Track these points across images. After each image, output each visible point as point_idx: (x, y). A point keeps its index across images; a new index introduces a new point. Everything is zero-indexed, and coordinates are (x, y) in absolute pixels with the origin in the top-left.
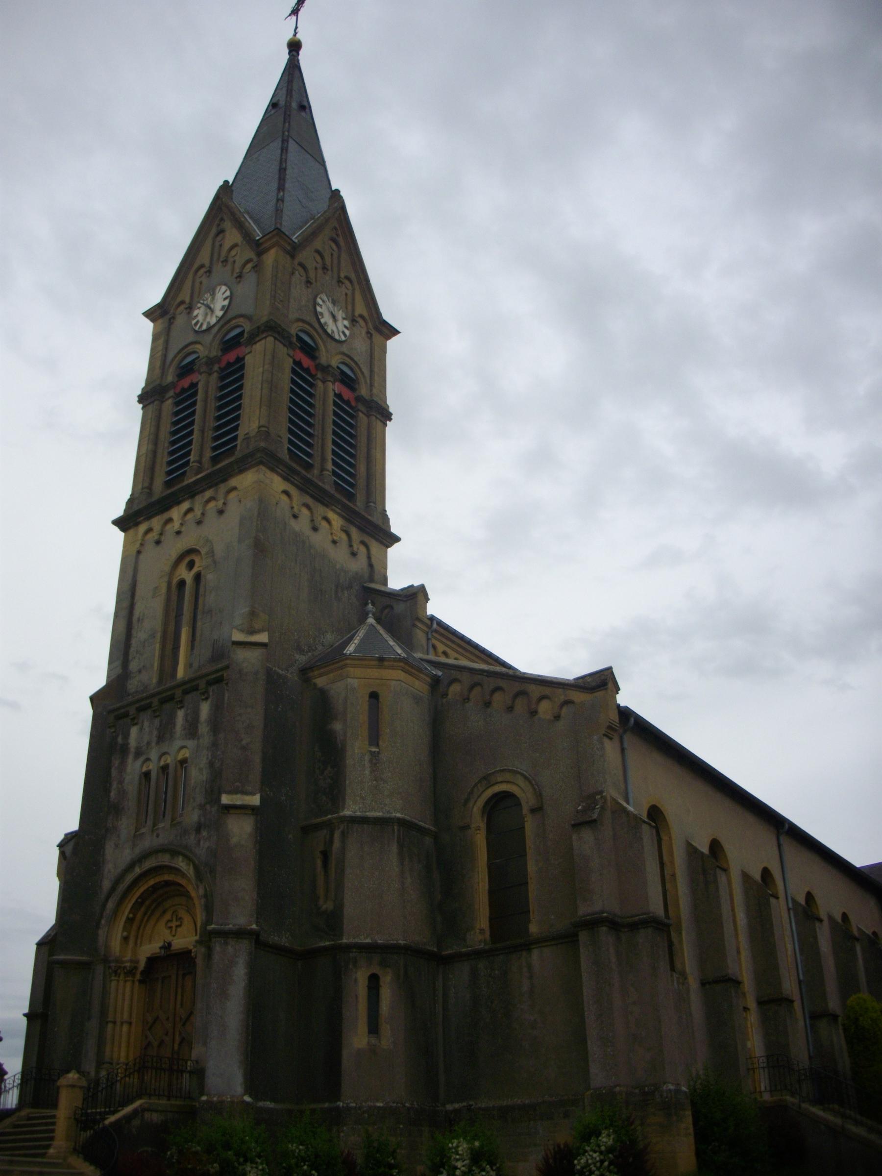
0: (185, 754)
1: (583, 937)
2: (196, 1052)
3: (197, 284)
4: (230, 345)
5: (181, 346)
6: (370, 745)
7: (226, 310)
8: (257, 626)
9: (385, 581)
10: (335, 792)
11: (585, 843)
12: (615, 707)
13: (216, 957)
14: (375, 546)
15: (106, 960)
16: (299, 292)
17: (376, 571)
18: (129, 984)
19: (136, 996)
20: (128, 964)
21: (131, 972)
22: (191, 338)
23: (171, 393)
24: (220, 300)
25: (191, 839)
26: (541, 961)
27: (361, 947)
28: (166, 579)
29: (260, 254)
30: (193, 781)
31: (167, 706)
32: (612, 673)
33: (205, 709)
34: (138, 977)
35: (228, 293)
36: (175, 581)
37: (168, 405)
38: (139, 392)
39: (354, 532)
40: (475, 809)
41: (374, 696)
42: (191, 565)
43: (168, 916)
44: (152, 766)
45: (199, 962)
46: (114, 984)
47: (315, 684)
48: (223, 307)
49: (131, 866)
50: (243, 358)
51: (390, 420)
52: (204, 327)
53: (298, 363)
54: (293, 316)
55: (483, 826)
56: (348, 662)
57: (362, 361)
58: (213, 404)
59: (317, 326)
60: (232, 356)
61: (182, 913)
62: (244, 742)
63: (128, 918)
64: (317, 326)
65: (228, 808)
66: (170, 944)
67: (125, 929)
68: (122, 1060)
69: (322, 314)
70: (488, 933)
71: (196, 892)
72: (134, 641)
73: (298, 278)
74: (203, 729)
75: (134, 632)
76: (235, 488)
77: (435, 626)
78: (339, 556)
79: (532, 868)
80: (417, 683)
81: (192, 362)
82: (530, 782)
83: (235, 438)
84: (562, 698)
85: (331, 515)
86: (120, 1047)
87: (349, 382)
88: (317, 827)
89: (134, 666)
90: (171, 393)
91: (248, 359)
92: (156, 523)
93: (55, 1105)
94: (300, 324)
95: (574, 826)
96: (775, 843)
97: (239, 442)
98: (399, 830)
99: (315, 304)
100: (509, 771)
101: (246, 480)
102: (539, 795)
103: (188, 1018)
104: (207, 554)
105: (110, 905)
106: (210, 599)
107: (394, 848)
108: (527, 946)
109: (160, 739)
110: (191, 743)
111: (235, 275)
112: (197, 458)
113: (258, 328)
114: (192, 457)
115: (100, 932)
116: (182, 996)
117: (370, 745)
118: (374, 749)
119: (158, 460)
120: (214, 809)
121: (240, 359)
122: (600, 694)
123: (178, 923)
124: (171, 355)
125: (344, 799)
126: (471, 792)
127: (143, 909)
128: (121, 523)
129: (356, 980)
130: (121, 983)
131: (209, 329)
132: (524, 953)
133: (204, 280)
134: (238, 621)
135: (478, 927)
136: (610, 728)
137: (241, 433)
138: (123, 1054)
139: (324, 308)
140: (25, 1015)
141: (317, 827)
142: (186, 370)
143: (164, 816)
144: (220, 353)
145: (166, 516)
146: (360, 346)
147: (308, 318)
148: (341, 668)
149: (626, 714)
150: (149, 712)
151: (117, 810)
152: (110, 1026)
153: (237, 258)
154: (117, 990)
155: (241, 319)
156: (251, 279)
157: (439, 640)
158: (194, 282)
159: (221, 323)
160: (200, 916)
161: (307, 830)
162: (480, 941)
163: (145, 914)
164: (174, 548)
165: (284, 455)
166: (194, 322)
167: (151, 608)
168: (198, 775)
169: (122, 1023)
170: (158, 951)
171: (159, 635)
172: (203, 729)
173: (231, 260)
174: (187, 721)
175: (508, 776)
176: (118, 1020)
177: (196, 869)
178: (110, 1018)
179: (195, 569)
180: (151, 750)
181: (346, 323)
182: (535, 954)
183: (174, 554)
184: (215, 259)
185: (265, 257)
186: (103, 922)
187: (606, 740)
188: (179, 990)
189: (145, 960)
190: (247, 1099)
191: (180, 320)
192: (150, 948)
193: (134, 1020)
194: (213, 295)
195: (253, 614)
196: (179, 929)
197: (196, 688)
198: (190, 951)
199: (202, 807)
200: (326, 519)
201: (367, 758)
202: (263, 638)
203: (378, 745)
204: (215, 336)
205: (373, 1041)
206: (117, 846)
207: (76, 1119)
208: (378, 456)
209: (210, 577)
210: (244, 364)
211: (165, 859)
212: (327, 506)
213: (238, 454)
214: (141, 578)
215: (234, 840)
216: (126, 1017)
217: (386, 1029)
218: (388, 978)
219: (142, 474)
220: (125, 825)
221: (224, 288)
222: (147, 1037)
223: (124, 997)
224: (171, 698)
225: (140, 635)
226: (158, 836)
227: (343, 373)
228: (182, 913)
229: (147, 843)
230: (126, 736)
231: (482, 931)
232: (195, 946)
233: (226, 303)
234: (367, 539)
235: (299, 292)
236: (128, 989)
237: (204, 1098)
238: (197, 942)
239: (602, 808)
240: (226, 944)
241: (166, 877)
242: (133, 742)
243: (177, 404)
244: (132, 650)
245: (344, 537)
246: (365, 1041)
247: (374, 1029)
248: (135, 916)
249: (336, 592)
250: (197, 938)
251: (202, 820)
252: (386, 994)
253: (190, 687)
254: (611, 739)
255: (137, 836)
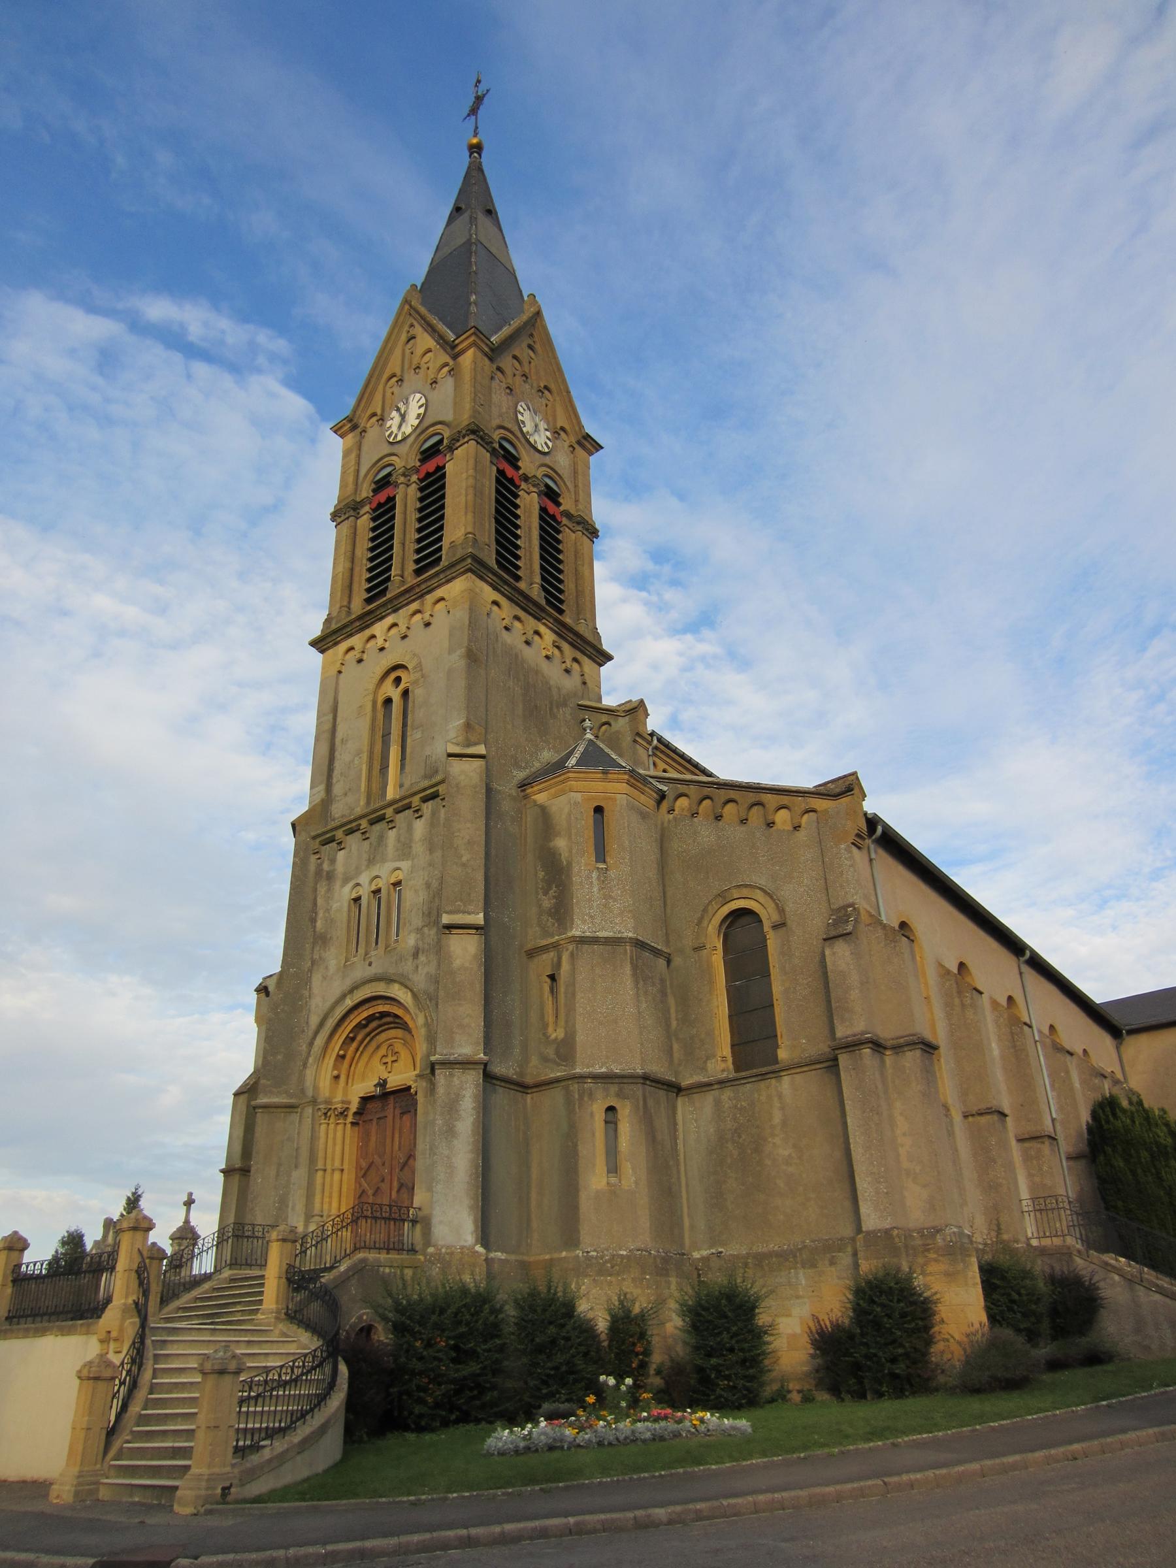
0: (399, 875)
1: (844, 1060)
2: (419, 1199)
3: (388, 394)
4: (428, 454)
5: (374, 460)
6: (597, 861)
7: (421, 418)
8: (473, 739)
9: (600, 699)
10: (561, 912)
11: (840, 956)
12: (862, 815)
13: (441, 1090)
14: (588, 664)
15: (314, 1102)
16: (500, 398)
17: (590, 687)
18: (340, 1127)
19: (347, 1141)
20: (339, 1106)
21: (343, 1114)
22: (387, 449)
23: (367, 508)
24: (414, 409)
25: (407, 967)
26: (789, 1095)
27: (596, 1077)
28: (371, 697)
29: (455, 357)
30: (408, 904)
31: (377, 827)
32: (857, 778)
33: (420, 827)
34: (350, 1119)
35: (423, 401)
36: (380, 700)
37: (365, 522)
38: (332, 510)
39: (566, 647)
40: (710, 927)
41: (599, 810)
42: (398, 680)
43: (382, 1051)
44: (364, 892)
45: (420, 1098)
46: (323, 1127)
47: (535, 801)
48: (419, 415)
49: (343, 997)
50: (444, 467)
51: (597, 537)
52: (399, 438)
53: (501, 472)
54: (496, 422)
55: (720, 946)
56: (570, 775)
57: (566, 473)
58: (413, 516)
59: (520, 435)
60: (431, 466)
61: (398, 1046)
62: (464, 859)
63: (338, 1055)
64: (520, 435)
65: (449, 927)
66: (385, 1081)
67: (335, 1067)
68: (334, 1212)
69: (523, 422)
70: (730, 1060)
71: (418, 1021)
72: (338, 765)
73: (498, 386)
74: (419, 848)
75: (337, 754)
76: (442, 599)
77: (655, 742)
78: (553, 673)
79: (777, 988)
80: (643, 798)
81: (389, 474)
82: (771, 897)
83: (440, 549)
84: (803, 807)
85: (542, 629)
86: (331, 1197)
87: (551, 495)
88: (544, 949)
89: (338, 789)
90: (367, 508)
91: (449, 468)
92: (357, 641)
93: (264, 1265)
94: (502, 431)
95: (825, 940)
96: (1016, 971)
97: (444, 552)
98: (632, 951)
99: (516, 412)
100: (746, 886)
101: (457, 587)
102: (781, 911)
103: (405, 1164)
104: (415, 668)
105: (320, 1041)
106: (418, 714)
107: (628, 970)
108: (776, 1074)
109: (371, 862)
110: (405, 865)
111: (430, 381)
112: (399, 572)
113: (459, 432)
114: (393, 572)
115: (308, 1072)
116: (400, 1137)
117: (597, 861)
118: (602, 866)
119: (356, 579)
120: (433, 932)
121: (440, 468)
122: (844, 800)
123: (394, 1058)
124: (363, 472)
125: (572, 920)
126: (705, 910)
127: (355, 1045)
128: (321, 644)
129: (592, 1115)
130: (332, 1126)
131: (404, 439)
132: (773, 1081)
133: (396, 390)
134: (452, 734)
135: (719, 1054)
136: (858, 835)
137: (445, 543)
138: (335, 1204)
139: (526, 417)
140: (222, 1171)
141: (544, 949)
142: (383, 484)
143: (377, 943)
144: (418, 464)
145: (367, 633)
146: (562, 461)
147: (509, 426)
148: (563, 782)
149: (872, 822)
150: (358, 834)
151: (322, 940)
152: (320, 1173)
153: (430, 365)
154: (327, 1134)
155: (439, 426)
156: (447, 385)
157: (660, 758)
158: (384, 392)
159: (418, 431)
160: (421, 1048)
161: (532, 953)
162: (723, 1071)
163: (357, 1050)
164: (378, 664)
165: (493, 563)
166: (387, 434)
167: (356, 731)
168: (415, 897)
169: (333, 1170)
170: (373, 1089)
171: (365, 756)
172: (419, 848)
173: (424, 367)
174: (399, 841)
175: (745, 892)
176: (329, 1167)
177: (415, 995)
178: (320, 1165)
179: (402, 686)
180: (359, 872)
181: (548, 434)
182: (786, 1080)
183: (379, 671)
184: (406, 366)
185: (461, 359)
186: (311, 1060)
187: (854, 849)
188: (397, 1135)
189: (358, 1100)
190: (479, 1248)
191: (373, 433)
192: (366, 1086)
193: (346, 1167)
194: (406, 403)
195: (468, 726)
196: (395, 1064)
197: (408, 807)
198: (409, 1088)
199: (419, 930)
200: (537, 633)
201: (595, 875)
202: (481, 749)
203: (604, 861)
204: (411, 446)
205: (613, 1180)
206: (324, 978)
207: (288, 1279)
208: (587, 573)
209: (417, 693)
210: (445, 474)
211: (380, 989)
212: (539, 620)
213: (444, 563)
214: (342, 698)
215: (457, 963)
216: (337, 1164)
217: (627, 1168)
218: (627, 1111)
219: (339, 594)
220: (333, 958)
221: (418, 396)
222: (360, 1185)
223: (338, 1144)
224: (382, 818)
225: (343, 757)
226: (370, 964)
227: (547, 486)
228: (398, 1046)
229: (360, 971)
230: (333, 861)
231: (724, 1059)
232: (416, 1081)
233: (422, 410)
234: (579, 656)
235: (500, 398)
236: (339, 1134)
237: (431, 1250)
238: (417, 1076)
239: (856, 920)
240: (451, 1075)
241: (381, 1008)
242: (340, 867)
243: (374, 519)
244: (336, 773)
245: (556, 652)
246: (604, 1181)
247: (613, 1168)
248: (346, 1052)
249: (551, 709)
250: (417, 1072)
251: (420, 944)
252: (626, 1127)
253: (403, 806)
254: (859, 848)
255: (347, 966)
